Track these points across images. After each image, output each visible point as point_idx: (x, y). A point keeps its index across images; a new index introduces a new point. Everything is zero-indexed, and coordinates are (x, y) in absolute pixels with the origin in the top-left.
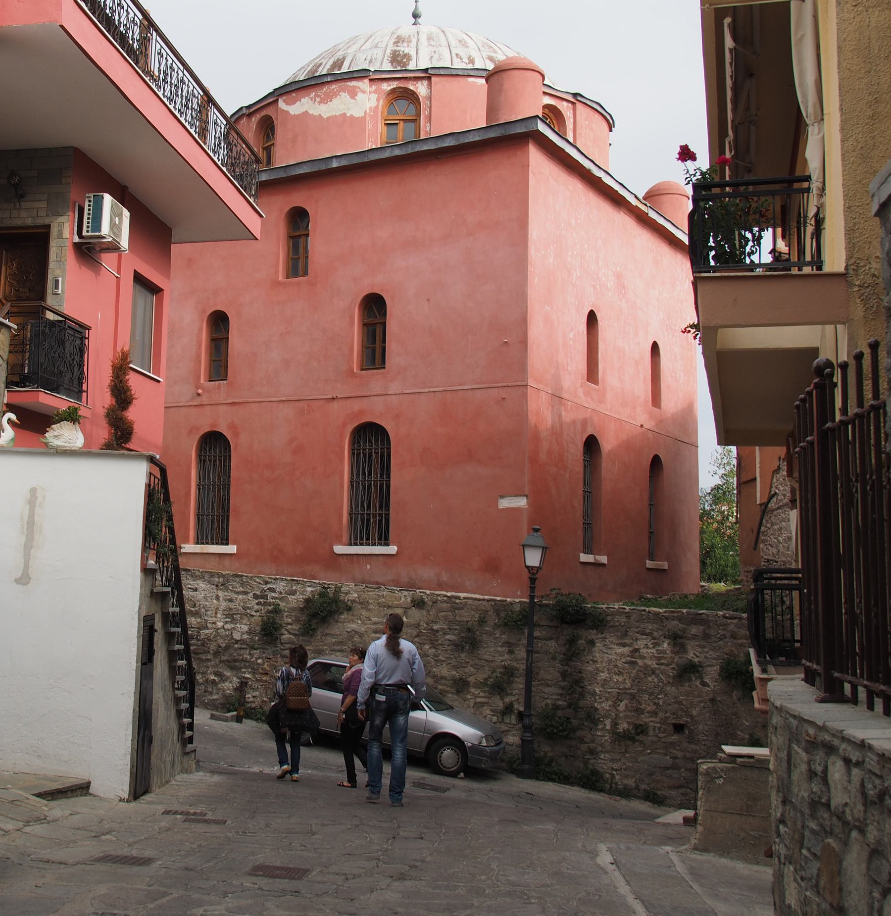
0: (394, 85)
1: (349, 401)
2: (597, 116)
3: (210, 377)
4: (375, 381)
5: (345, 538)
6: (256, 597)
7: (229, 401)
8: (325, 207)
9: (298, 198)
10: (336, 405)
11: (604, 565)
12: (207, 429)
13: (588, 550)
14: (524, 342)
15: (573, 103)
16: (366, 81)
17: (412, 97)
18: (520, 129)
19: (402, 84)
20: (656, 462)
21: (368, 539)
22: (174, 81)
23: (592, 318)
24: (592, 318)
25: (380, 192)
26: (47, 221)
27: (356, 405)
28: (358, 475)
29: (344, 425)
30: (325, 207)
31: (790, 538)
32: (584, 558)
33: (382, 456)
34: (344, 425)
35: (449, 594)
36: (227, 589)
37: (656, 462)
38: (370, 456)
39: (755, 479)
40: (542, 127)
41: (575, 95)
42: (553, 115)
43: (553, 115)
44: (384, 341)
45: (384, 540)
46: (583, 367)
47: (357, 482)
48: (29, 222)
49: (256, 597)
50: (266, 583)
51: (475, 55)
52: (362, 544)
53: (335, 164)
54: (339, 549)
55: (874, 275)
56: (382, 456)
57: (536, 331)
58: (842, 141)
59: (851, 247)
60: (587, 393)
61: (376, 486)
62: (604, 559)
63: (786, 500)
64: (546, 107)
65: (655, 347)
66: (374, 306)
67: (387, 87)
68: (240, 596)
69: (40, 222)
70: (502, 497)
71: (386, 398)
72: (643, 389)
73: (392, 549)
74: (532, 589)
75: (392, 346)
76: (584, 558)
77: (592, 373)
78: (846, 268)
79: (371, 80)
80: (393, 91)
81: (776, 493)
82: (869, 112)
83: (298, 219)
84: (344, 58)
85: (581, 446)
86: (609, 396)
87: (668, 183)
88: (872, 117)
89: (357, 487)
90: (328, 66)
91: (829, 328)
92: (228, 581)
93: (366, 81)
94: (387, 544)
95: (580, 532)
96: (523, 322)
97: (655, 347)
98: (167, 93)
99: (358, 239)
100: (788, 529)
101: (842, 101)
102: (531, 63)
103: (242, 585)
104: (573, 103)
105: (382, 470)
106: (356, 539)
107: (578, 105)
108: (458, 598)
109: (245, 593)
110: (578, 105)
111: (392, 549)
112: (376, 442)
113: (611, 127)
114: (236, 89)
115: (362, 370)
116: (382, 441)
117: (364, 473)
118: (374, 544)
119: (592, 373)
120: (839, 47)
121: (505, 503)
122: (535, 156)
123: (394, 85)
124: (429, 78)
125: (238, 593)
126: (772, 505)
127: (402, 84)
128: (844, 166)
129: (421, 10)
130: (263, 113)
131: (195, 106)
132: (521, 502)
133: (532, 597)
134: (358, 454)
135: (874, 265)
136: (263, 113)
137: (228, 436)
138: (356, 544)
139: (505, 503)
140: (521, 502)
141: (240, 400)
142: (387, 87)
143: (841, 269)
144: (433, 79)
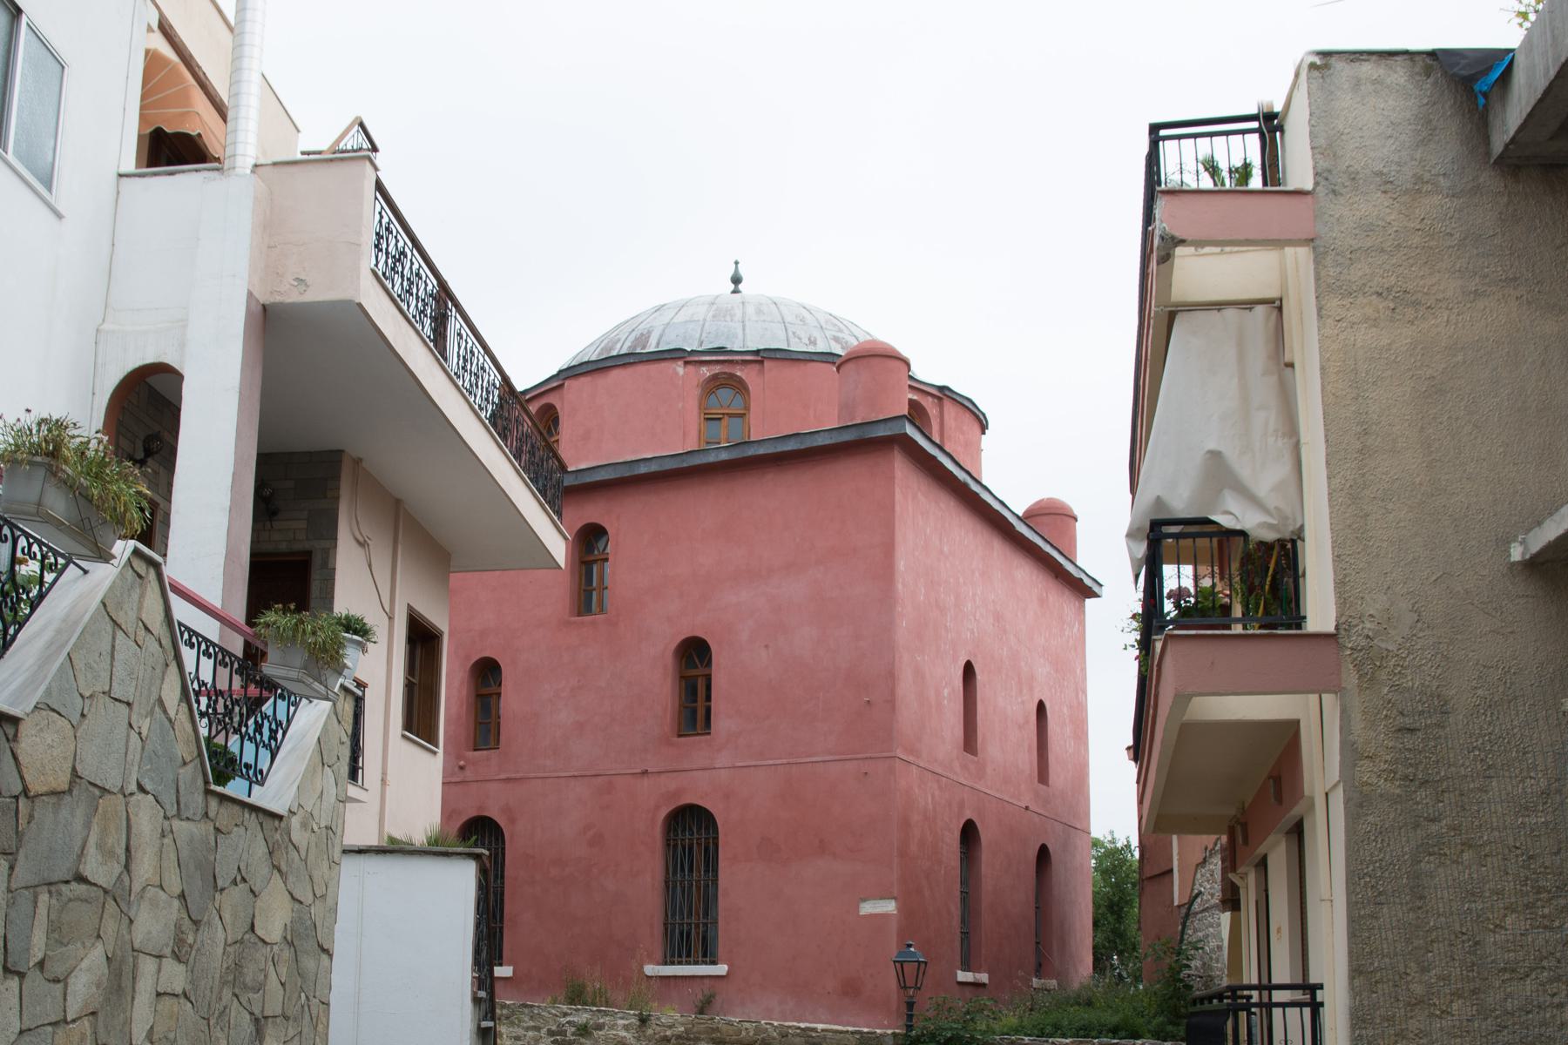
0: (717, 369)
1: (663, 776)
2: (968, 415)
3: (475, 743)
4: (697, 750)
5: (659, 954)
6: (551, 1033)
7: (503, 776)
8: (626, 522)
9: (593, 511)
10: (646, 782)
11: (983, 985)
12: (473, 813)
13: (966, 967)
14: (891, 702)
15: (940, 399)
16: (681, 363)
17: (740, 386)
18: (882, 432)
19: (727, 369)
20: (1043, 854)
21: (688, 955)
22: (474, 369)
23: (969, 670)
24: (969, 670)
25: (703, 507)
26: (307, 546)
27: (671, 783)
28: (675, 873)
29: (657, 807)
30: (626, 522)
31: (1220, 948)
32: (963, 976)
33: (707, 849)
34: (657, 807)
35: (802, 1025)
36: (512, 1024)
37: (1043, 854)
38: (691, 849)
39: (1171, 871)
40: (910, 430)
41: (942, 389)
42: (916, 413)
43: (916, 413)
44: (708, 698)
45: (709, 957)
46: (959, 731)
47: (675, 883)
48: (283, 547)
49: (551, 1033)
50: (565, 1015)
51: (817, 334)
52: (680, 963)
53: (643, 469)
54: (651, 969)
55: (1368, 636)
56: (707, 849)
57: (906, 687)
58: (1329, 478)
59: (1343, 602)
60: (964, 767)
61: (698, 888)
62: (984, 977)
63: (1216, 901)
64: (912, 403)
65: (1041, 707)
66: (694, 653)
67: (706, 372)
68: (530, 1033)
69: (298, 547)
70: (864, 900)
71: (711, 773)
72: (1026, 760)
73: (721, 969)
74: (910, 1017)
75: (717, 704)
76: (963, 976)
77: (970, 741)
78: (1337, 628)
79: (686, 363)
80: (714, 377)
81: (1200, 893)
82: (1359, 446)
83: (589, 540)
84: (649, 332)
85: (957, 834)
86: (989, 770)
87: (1051, 501)
88: (1360, 451)
89: (675, 887)
90: (628, 344)
91: (1314, 698)
92: (513, 1013)
93: (681, 363)
94: (714, 963)
95: (958, 944)
96: (891, 676)
97: (1041, 707)
98: (467, 384)
99: (677, 564)
100: (1218, 936)
101: (1326, 430)
102: (894, 350)
103: (532, 1018)
104: (940, 399)
105: (707, 866)
106: (673, 956)
107: (947, 402)
108: (814, 1030)
109: (538, 1029)
110: (947, 402)
111: (721, 969)
112: (699, 829)
113: (983, 428)
114: (528, 371)
115: (680, 736)
116: (707, 828)
117: (683, 869)
118: (696, 963)
119: (970, 741)
120: (1323, 369)
121: (867, 908)
122: (900, 466)
123: (717, 369)
124: (761, 362)
125: (527, 1029)
126: (1196, 907)
127: (727, 369)
128: (1331, 506)
129: (742, 271)
130: (544, 401)
131: (496, 400)
132: (890, 907)
133: (909, 1028)
134: (675, 846)
135: (1368, 625)
136: (544, 401)
137: (502, 825)
138: (673, 963)
139: (867, 908)
140: (890, 907)
141: (518, 775)
142: (706, 372)
143: (1331, 629)
144: (766, 363)
